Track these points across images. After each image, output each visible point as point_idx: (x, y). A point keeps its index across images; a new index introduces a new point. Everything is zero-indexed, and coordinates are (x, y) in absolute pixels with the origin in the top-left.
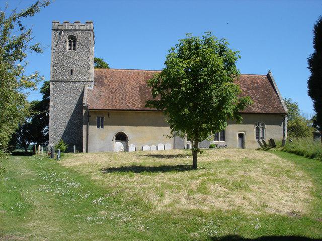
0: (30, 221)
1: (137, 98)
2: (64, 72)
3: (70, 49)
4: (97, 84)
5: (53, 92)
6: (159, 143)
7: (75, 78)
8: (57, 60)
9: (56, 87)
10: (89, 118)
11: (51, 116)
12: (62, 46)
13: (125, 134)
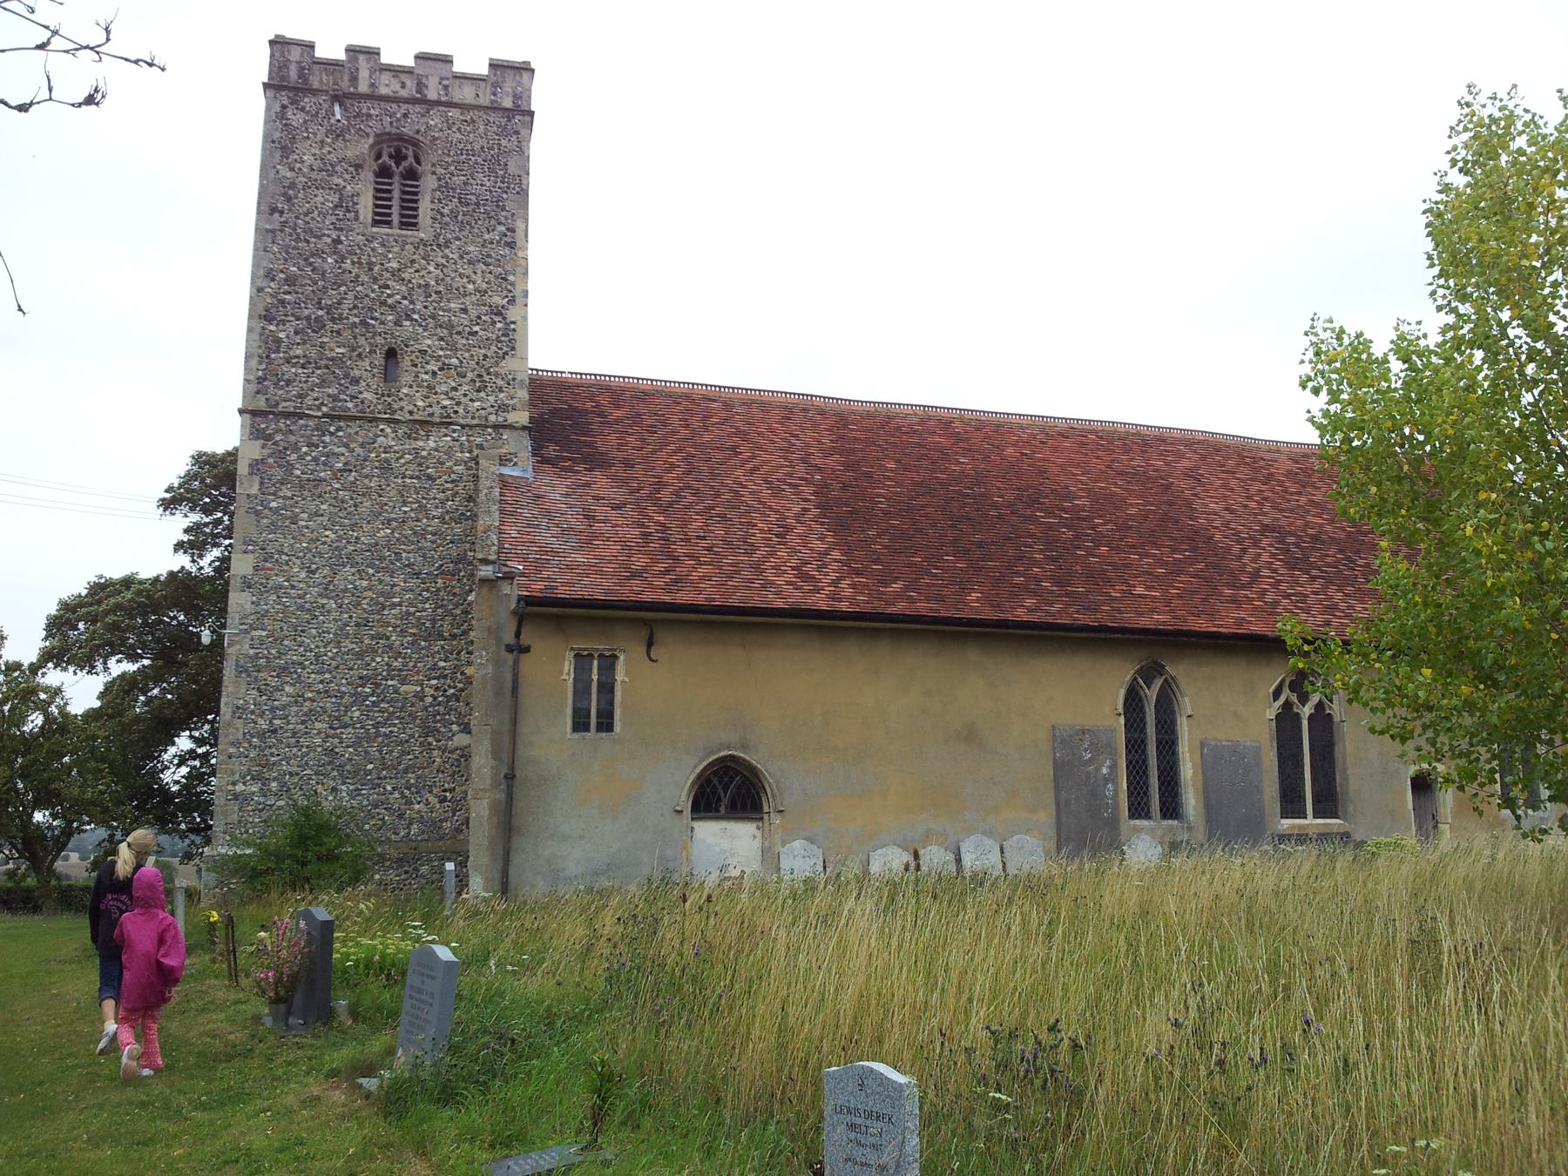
0: (175, 928)
1: (819, 546)
2: (338, 361)
3: (381, 219)
4: (551, 450)
5: (255, 490)
6: (970, 831)
7: (412, 399)
8: (290, 281)
9: (280, 454)
10: (516, 662)
11: (237, 649)
12: (335, 198)
13: (753, 771)
